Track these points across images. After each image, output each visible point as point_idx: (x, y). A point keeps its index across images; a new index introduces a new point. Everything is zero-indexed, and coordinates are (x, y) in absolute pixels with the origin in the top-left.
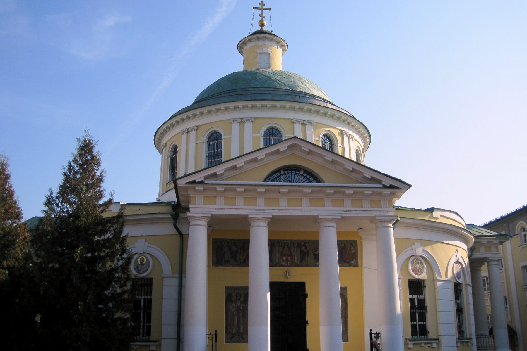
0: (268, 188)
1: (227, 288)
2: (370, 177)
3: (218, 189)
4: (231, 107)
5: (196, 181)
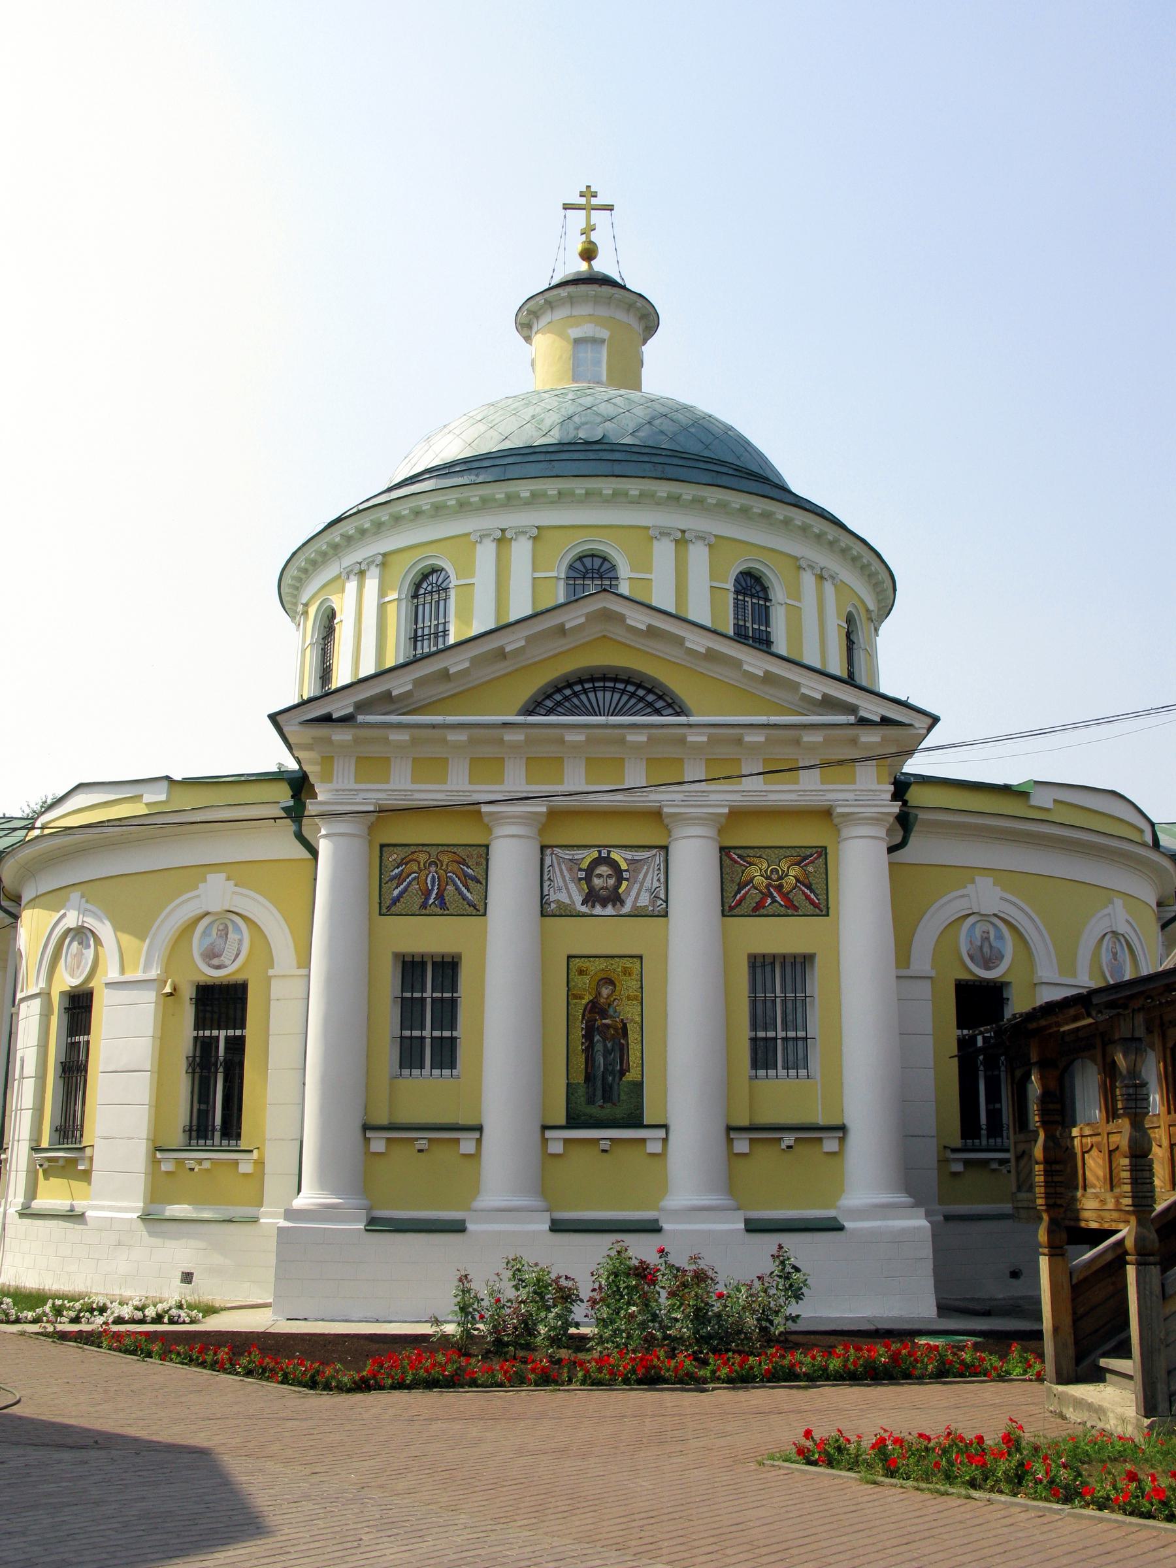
0: (532, 731)
1: (956, 980)
3: (690, 739)
4: (522, 495)
5: (334, 716)
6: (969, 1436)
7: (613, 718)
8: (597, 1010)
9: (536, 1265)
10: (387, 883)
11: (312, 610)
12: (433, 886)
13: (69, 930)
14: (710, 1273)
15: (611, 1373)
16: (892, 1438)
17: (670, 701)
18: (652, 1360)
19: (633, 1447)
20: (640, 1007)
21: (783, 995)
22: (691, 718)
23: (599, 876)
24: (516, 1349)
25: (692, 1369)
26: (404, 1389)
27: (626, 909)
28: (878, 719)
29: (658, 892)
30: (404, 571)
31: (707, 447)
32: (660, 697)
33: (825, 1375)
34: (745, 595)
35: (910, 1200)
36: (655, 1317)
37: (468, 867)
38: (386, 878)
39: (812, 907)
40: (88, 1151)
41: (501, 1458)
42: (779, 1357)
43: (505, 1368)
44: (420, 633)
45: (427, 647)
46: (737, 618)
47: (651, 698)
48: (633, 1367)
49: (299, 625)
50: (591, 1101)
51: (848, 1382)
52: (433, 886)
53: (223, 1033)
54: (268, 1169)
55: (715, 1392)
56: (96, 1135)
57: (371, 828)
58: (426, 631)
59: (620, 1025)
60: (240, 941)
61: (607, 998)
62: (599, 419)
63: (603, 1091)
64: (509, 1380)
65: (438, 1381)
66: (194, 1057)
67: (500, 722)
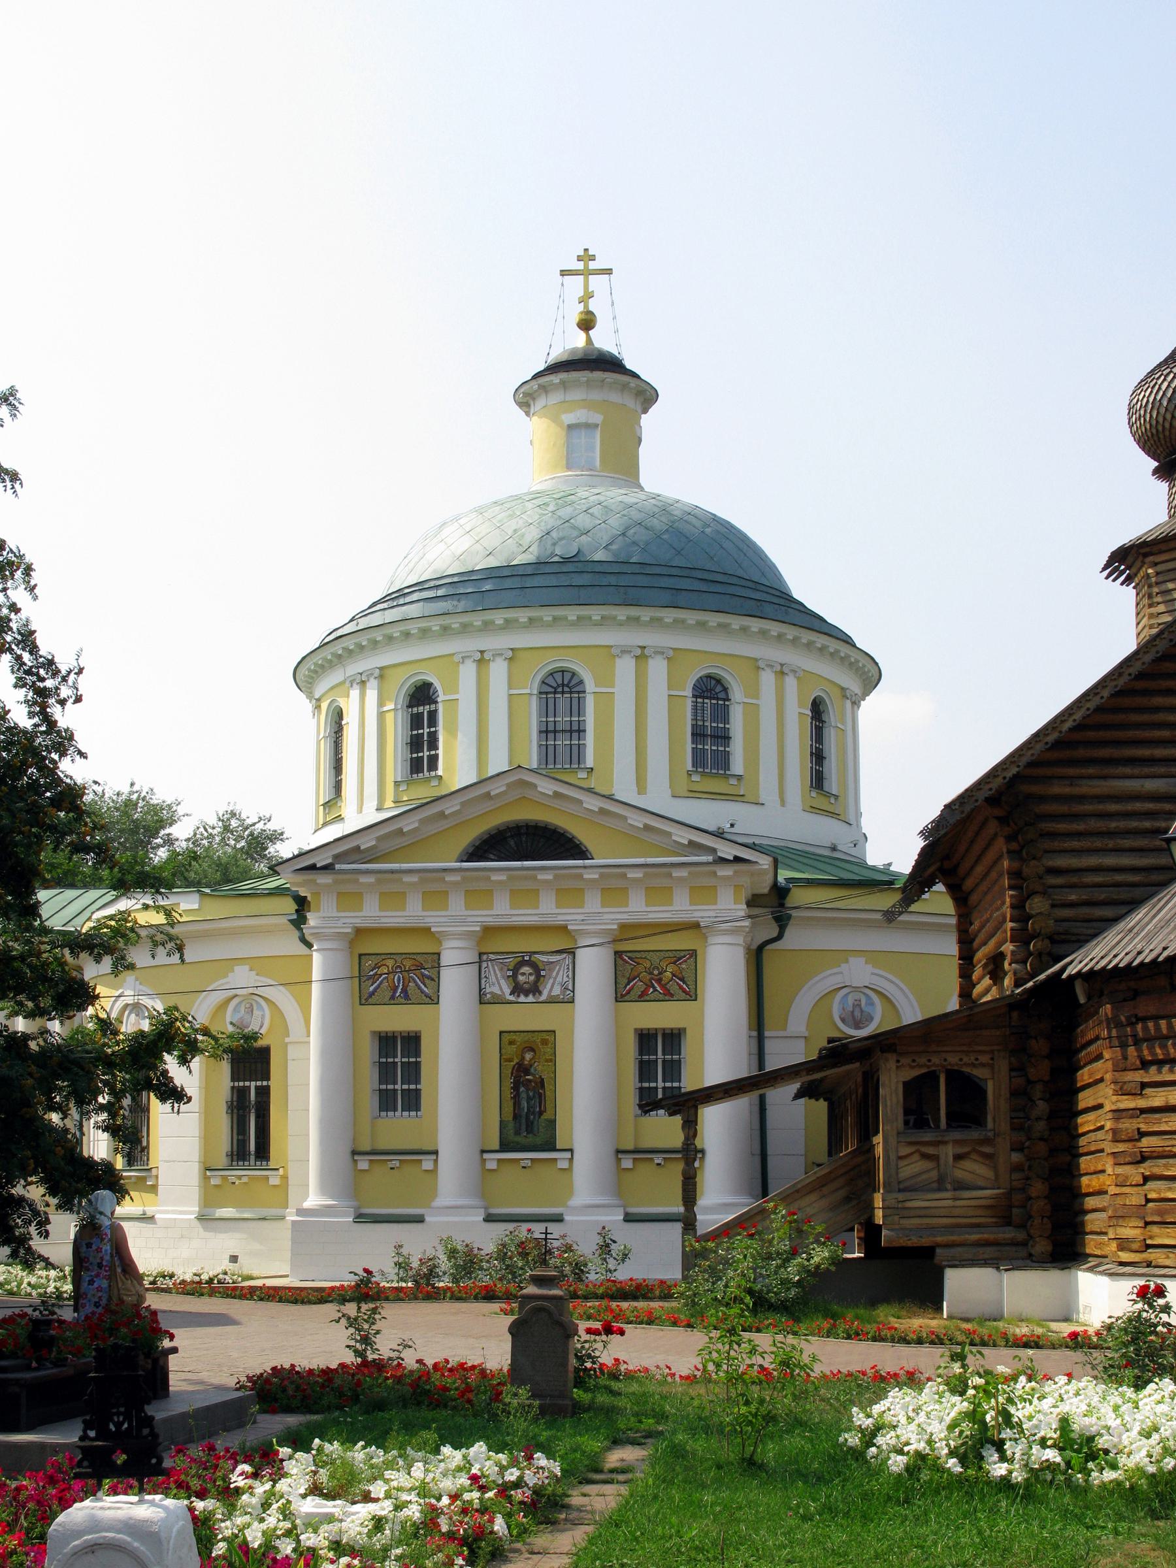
11: (324, 705)
12: (399, 983)
13: (127, 1005)
23: (523, 974)
27: (543, 997)
30: (401, 684)
31: (679, 553)
34: (704, 698)
40: (154, 1172)
50: (517, 1133)
52: (399, 983)
53: (253, 1084)
56: (160, 1159)
59: (539, 1080)
60: (263, 1016)
62: (575, 533)
66: (232, 1101)
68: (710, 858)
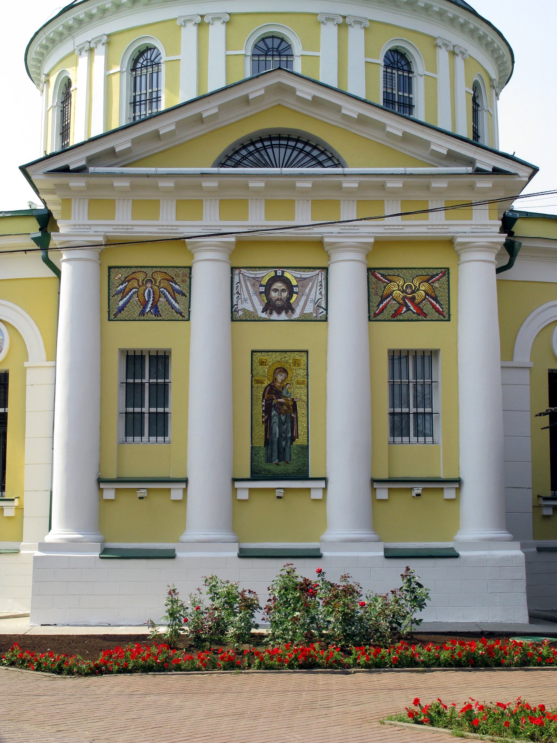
1: (549, 370)
2: (445, 152)
3: (345, 185)
5: (71, 168)
6: (534, 704)
7: (284, 169)
8: (274, 392)
9: (228, 582)
10: (114, 296)
11: (53, 79)
12: (149, 298)
14: (357, 588)
15: (279, 660)
16: (478, 706)
17: (330, 156)
18: (310, 651)
19: (292, 711)
20: (306, 390)
21: (415, 381)
22: (346, 169)
23: (276, 290)
24: (211, 644)
25: (339, 658)
26: (128, 673)
27: (296, 315)
28: (491, 170)
29: (320, 302)
32: (323, 153)
33: (438, 663)
34: (393, 68)
35: (508, 535)
36: (313, 620)
37: (176, 283)
38: (113, 293)
39: (437, 314)
41: (195, 719)
42: (404, 649)
43: (202, 657)
44: (138, 99)
45: (144, 111)
46: (386, 87)
47: (315, 153)
48: (296, 656)
49: (43, 91)
50: (269, 460)
51: (454, 668)
52: (149, 298)
54: (26, 513)
55: (356, 674)
57: (101, 254)
58: (143, 98)
59: (291, 403)
61: (281, 383)
63: (278, 452)
64: (205, 665)
65: (152, 667)
67: (199, 173)
68: (470, 169)
